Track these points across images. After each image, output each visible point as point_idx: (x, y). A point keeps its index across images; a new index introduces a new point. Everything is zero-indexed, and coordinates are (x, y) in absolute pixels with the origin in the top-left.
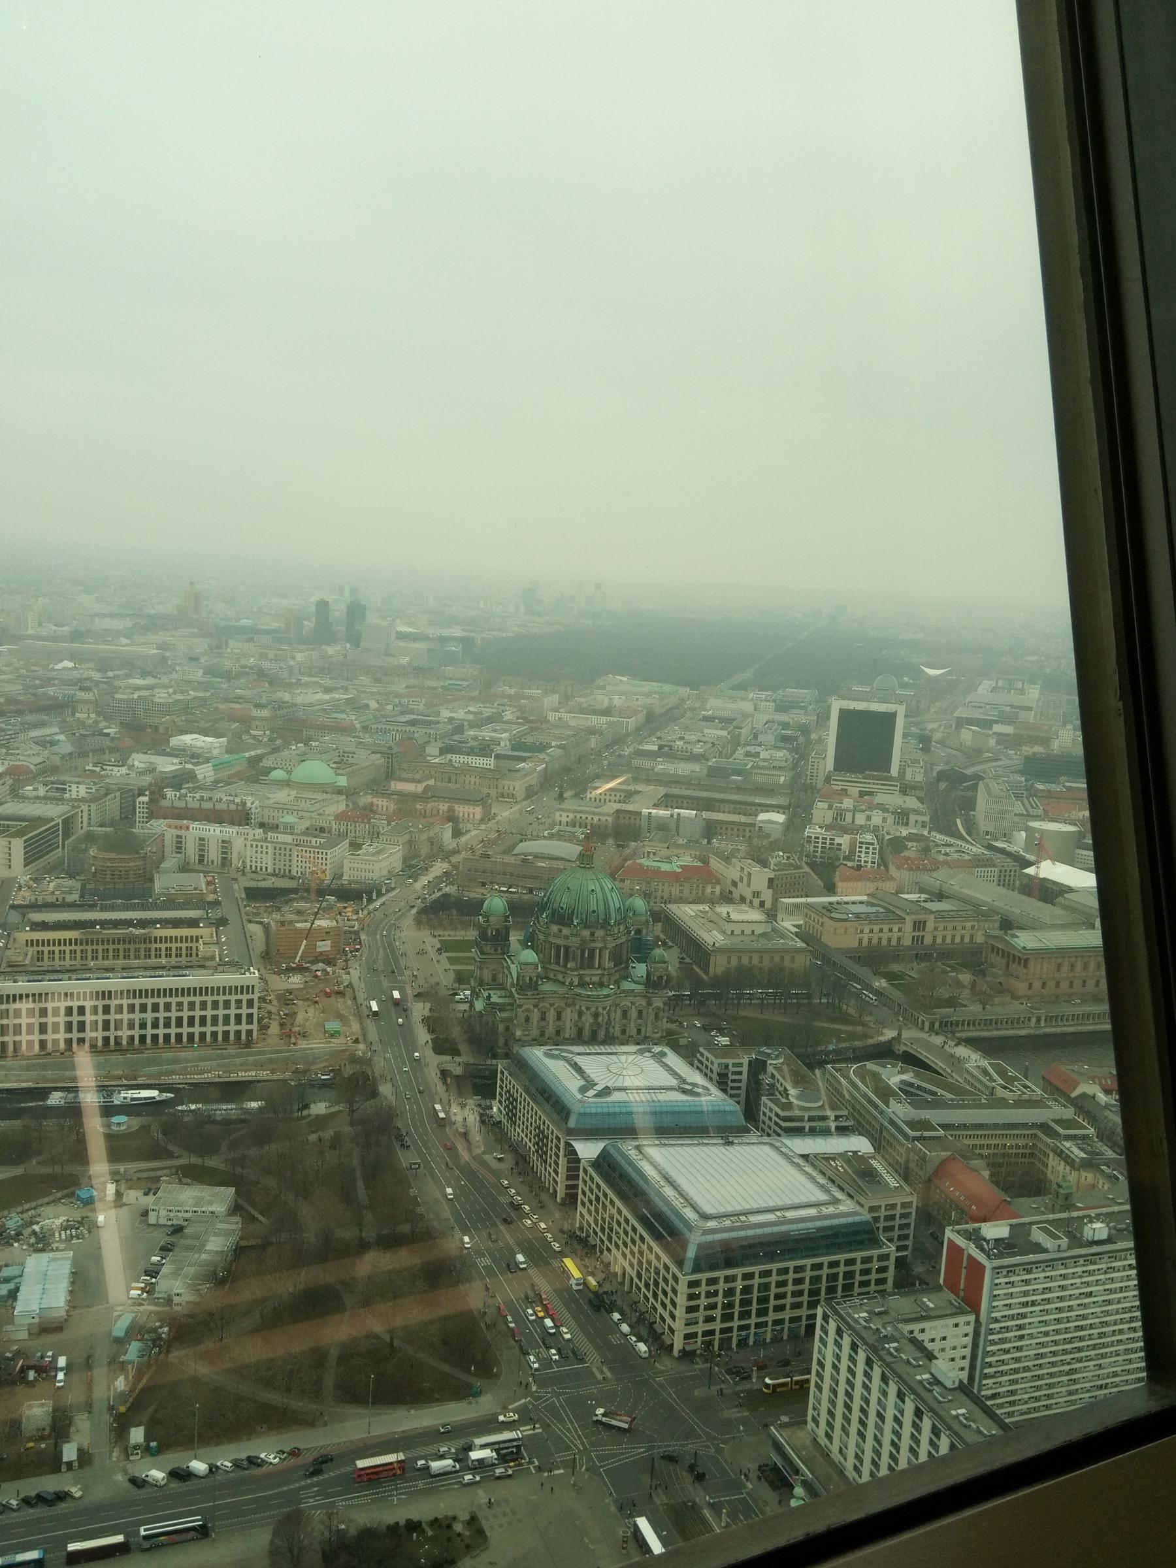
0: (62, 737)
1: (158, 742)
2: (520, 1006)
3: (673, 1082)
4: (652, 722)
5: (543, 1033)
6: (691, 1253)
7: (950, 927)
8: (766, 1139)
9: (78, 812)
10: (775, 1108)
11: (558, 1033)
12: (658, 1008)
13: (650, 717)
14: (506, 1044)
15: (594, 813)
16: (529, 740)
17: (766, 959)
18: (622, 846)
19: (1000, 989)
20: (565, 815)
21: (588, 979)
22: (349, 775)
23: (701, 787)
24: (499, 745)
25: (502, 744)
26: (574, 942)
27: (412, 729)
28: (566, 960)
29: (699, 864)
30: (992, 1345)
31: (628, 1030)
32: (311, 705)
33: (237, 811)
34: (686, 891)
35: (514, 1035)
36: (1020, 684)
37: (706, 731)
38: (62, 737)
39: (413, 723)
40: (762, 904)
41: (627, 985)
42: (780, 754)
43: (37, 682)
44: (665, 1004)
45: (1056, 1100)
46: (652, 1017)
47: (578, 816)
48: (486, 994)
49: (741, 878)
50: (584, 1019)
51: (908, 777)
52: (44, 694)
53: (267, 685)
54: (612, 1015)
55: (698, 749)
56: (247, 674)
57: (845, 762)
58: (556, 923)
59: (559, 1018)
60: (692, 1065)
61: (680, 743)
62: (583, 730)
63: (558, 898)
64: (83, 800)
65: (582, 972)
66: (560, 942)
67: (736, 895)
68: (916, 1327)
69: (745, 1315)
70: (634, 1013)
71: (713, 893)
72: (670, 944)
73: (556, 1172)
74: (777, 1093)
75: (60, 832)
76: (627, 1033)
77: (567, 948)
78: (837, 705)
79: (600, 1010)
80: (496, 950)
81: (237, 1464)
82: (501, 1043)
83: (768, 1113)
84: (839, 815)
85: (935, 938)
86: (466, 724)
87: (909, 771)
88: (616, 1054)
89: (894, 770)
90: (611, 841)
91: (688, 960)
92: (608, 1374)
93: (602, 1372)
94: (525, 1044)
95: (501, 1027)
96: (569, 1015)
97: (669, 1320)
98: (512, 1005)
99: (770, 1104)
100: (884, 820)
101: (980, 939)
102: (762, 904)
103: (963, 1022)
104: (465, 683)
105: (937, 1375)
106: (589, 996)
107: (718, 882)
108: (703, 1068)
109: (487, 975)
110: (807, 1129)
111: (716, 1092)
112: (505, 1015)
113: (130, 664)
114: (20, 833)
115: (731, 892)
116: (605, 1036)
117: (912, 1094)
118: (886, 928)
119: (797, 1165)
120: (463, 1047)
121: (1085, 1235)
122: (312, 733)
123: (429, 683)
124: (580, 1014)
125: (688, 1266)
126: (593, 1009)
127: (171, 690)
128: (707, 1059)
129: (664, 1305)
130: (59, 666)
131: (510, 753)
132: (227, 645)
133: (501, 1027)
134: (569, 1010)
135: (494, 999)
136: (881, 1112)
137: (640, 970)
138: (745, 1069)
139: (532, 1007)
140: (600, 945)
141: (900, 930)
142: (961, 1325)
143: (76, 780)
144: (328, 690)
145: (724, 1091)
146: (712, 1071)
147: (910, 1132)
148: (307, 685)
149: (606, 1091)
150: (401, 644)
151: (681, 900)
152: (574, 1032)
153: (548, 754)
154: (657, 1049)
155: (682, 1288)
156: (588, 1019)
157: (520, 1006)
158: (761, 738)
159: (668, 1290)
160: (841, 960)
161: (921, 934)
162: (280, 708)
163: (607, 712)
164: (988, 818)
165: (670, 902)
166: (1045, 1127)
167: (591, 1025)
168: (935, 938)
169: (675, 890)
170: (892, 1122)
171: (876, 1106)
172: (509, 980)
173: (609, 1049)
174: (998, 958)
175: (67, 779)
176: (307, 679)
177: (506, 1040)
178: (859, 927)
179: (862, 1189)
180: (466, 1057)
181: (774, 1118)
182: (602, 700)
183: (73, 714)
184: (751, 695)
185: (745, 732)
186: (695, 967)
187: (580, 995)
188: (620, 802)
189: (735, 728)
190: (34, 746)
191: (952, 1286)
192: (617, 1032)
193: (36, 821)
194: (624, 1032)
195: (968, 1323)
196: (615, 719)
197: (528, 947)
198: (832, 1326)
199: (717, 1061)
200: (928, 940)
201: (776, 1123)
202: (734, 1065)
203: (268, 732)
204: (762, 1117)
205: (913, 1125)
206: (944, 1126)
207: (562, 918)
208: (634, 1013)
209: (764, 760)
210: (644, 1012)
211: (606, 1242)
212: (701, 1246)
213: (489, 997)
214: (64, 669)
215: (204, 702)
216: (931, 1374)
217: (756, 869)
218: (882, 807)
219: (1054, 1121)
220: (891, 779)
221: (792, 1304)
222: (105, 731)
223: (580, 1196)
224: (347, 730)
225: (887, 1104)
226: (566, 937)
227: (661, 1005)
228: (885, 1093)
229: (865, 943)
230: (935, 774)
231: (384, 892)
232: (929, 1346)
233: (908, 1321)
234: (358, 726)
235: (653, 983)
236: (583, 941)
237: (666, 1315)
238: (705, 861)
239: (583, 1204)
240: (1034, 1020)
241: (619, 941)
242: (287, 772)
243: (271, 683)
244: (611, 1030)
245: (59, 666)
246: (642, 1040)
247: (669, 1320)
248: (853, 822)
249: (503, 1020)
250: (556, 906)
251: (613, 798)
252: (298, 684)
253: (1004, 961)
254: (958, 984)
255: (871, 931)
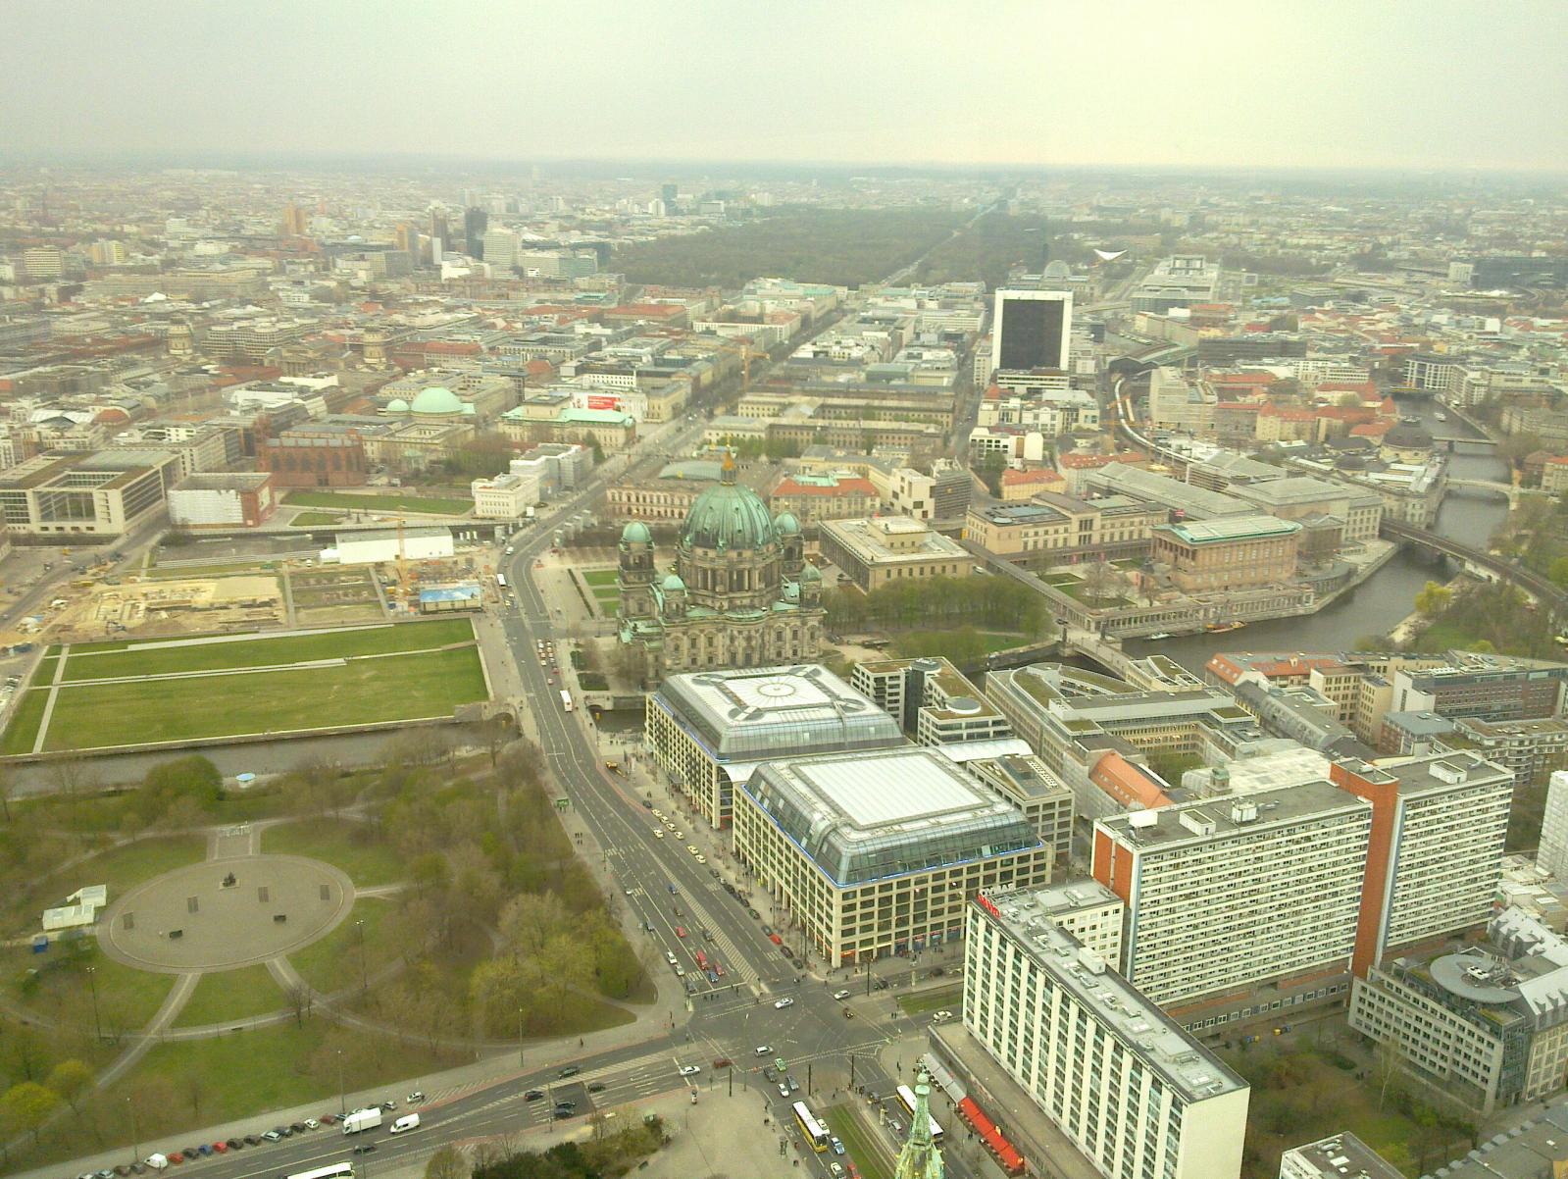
0: (157, 377)
1: (265, 376)
2: (668, 635)
3: (827, 700)
4: (809, 328)
5: (694, 661)
6: (844, 866)
7: (1118, 525)
8: (923, 749)
9: (177, 459)
10: (933, 718)
11: (710, 660)
12: (813, 627)
13: (805, 322)
14: (657, 673)
15: (745, 430)
16: (673, 355)
17: (927, 570)
18: (776, 463)
19: (1173, 585)
20: (714, 433)
21: (738, 602)
22: (477, 402)
23: (859, 395)
24: (641, 360)
25: (644, 359)
26: (720, 564)
27: (544, 348)
28: (714, 585)
29: (858, 476)
30: (1142, 930)
31: (783, 651)
32: (431, 327)
33: (353, 447)
34: (845, 507)
35: (664, 664)
36: (1199, 262)
37: (865, 333)
38: (157, 377)
39: (544, 341)
40: (925, 514)
41: (780, 606)
42: (943, 354)
43: (125, 318)
44: (820, 623)
45: (1217, 689)
46: (808, 637)
47: (729, 433)
48: (632, 625)
49: (902, 488)
50: (736, 643)
51: (1079, 370)
52: (135, 332)
53: (381, 307)
54: (766, 638)
55: (856, 353)
56: (359, 296)
57: (1008, 361)
58: (701, 546)
59: (711, 644)
60: (848, 682)
61: (836, 348)
62: (731, 340)
63: (701, 519)
64: (183, 444)
65: (731, 595)
66: (706, 565)
67: (898, 508)
68: (1065, 918)
69: (902, 922)
70: (788, 634)
71: (873, 506)
72: (828, 561)
73: (710, 799)
74: (934, 703)
75: (162, 480)
76: (783, 655)
77: (714, 572)
78: (1001, 296)
79: (753, 633)
80: (640, 578)
81: (172, 1160)
82: (651, 674)
83: (925, 723)
84: (1005, 415)
85: (1102, 538)
86: (603, 339)
87: (1079, 363)
88: (774, 675)
89: (1064, 365)
90: (764, 458)
91: (846, 577)
92: (766, 990)
93: (759, 988)
94: (675, 672)
95: (650, 658)
96: (721, 640)
97: (826, 933)
98: (659, 634)
99: (927, 714)
100: (1053, 418)
101: (1148, 534)
102: (925, 514)
103: (1130, 619)
104: (602, 295)
105: (1083, 962)
106: (740, 620)
107: (877, 494)
108: (859, 684)
109: (633, 606)
110: (965, 737)
111: (871, 709)
112: (654, 644)
113: (228, 296)
114: (114, 485)
115: (892, 504)
116: (760, 659)
117: (1072, 694)
118: (1051, 530)
119: (951, 773)
120: (610, 679)
121: (1233, 817)
122: (435, 358)
123: (562, 296)
124: (732, 639)
125: (842, 878)
126: (745, 633)
127: (274, 319)
128: (863, 674)
129: (821, 919)
130: (150, 299)
131: (653, 369)
132: (335, 266)
133: (650, 658)
134: (720, 635)
135: (642, 628)
136: (1042, 714)
137: (793, 589)
138: (902, 682)
139: (680, 635)
140: (747, 566)
141: (1066, 530)
142: (1111, 913)
143: (174, 422)
144: (449, 309)
145: (881, 705)
146: (868, 686)
147: (1068, 731)
148: (426, 304)
149: (758, 713)
150: (530, 253)
151: (839, 516)
152: (727, 658)
153: (695, 369)
154: (810, 668)
155: (837, 900)
156: (740, 643)
157: (668, 635)
158: (924, 338)
159: (824, 903)
160: (1005, 565)
161: (1087, 533)
162: (397, 332)
163: (758, 319)
164: (1161, 409)
165: (828, 519)
166: (1204, 716)
167: (745, 649)
168: (1102, 538)
169: (833, 506)
170: (1051, 723)
171: (1036, 709)
172: (657, 609)
173: (765, 671)
174: (1166, 552)
175: (165, 422)
176: (425, 298)
177: (657, 671)
178: (1024, 531)
179: (1015, 787)
180: (616, 691)
181: (932, 728)
182: (751, 306)
183: (168, 351)
184: (914, 292)
185: (907, 335)
186: (855, 584)
187: (730, 619)
188: (774, 415)
189: (897, 328)
190: (126, 388)
191: (1100, 875)
192: (771, 653)
193: (133, 470)
194: (779, 654)
195: (1117, 911)
196: (767, 326)
197: (673, 573)
198: (982, 925)
199: (873, 676)
200: (1096, 539)
201: (934, 733)
202: (891, 678)
203: (384, 359)
204: (919, 728)
205: (1071, 724)
206: (1103, 724)
207: (706, 540)
208: (788, 634)
209: (926, 362)
210: (800, 633)
211: (762, 863)
212: (853, 858)
213: (635, 627)
214: (156, 302)
215: (311, 331)
216: (1079, 961)
217: (917, 478)
218: (1050, 404)
219: (1214, 710)
220: (1061, 373)
221: (950, 908)
222: (204, 368)
223: (735, 820)
224: (473, 351)
225: (1047, 706)
226: (712, 560)
227: (816, 623)
228: (1044, 694)
229: (1030, 547)
230: (1107, 367)
231: (521, 525)
232: (1077, 935)
233: (1057, 913)
234: (483, 347)
235: (805, 602)
236: (731, 562)
237: (823, 928)
238: (865, 474)
239: (738, 827)
240: (1202, 612)
241: (769, 561)
242: (408, 402)
243: (385, 305)
244: (766, 653)
245: (150, 299)
246: (797, 660)
247: (826, 933)
248: (1020, 421)
249: (651, 650)
250: (699, 528)
251: (766, 412)
252: (417, 303)
253: (1172, 555)
254: (1126, 583)
255: (1036, 534)
